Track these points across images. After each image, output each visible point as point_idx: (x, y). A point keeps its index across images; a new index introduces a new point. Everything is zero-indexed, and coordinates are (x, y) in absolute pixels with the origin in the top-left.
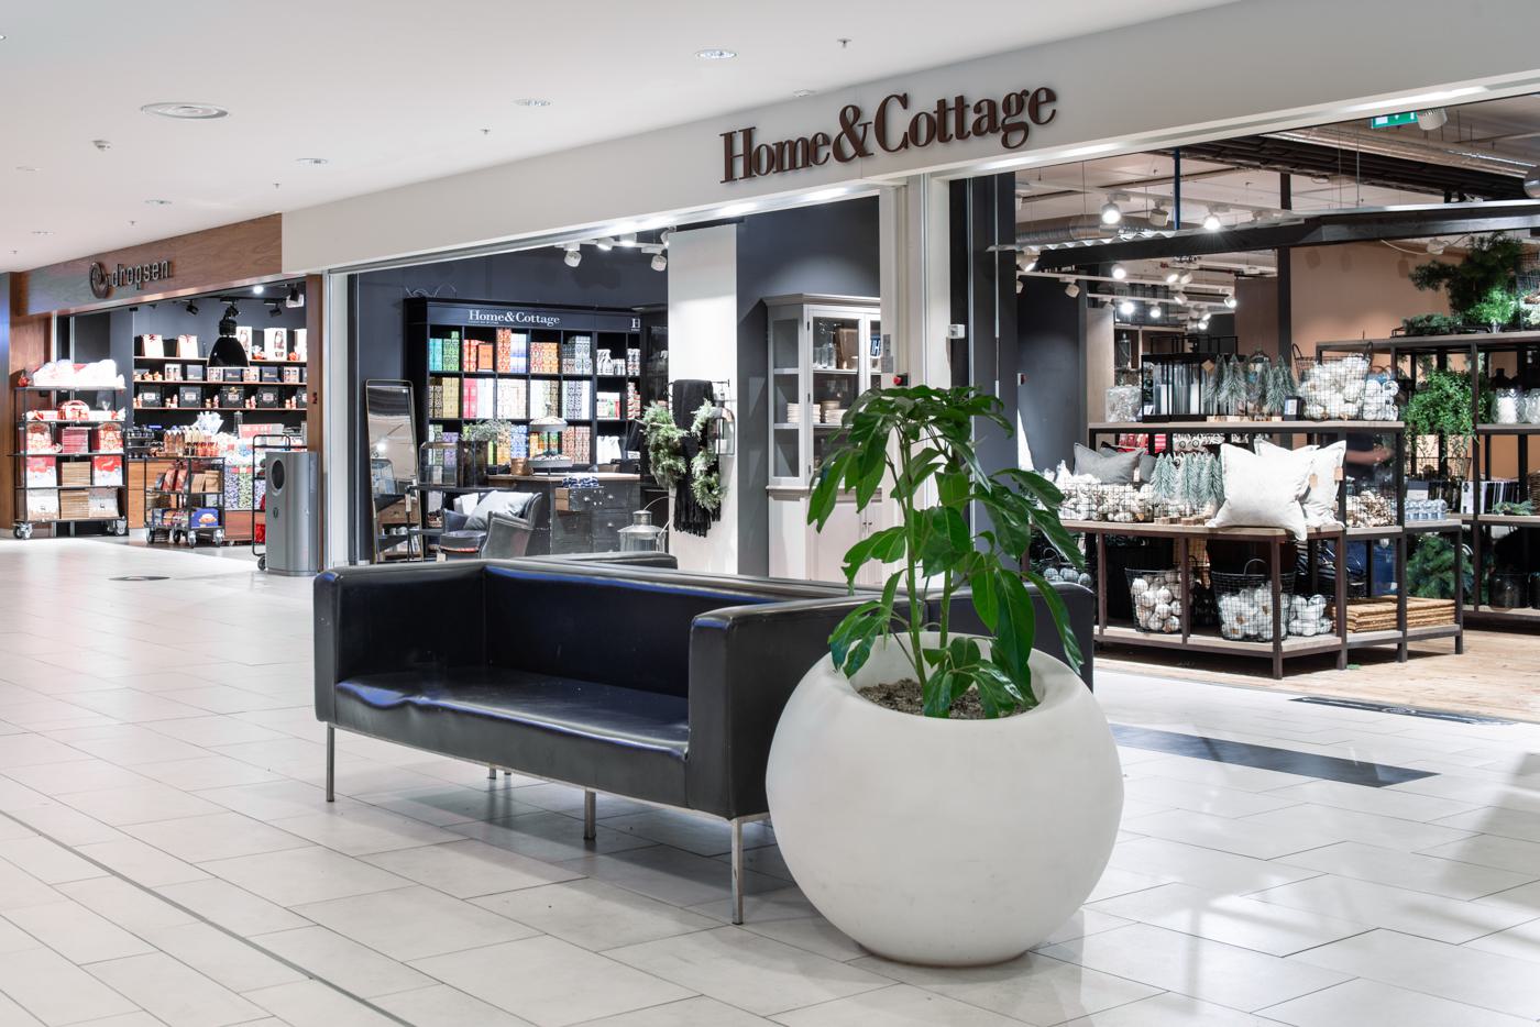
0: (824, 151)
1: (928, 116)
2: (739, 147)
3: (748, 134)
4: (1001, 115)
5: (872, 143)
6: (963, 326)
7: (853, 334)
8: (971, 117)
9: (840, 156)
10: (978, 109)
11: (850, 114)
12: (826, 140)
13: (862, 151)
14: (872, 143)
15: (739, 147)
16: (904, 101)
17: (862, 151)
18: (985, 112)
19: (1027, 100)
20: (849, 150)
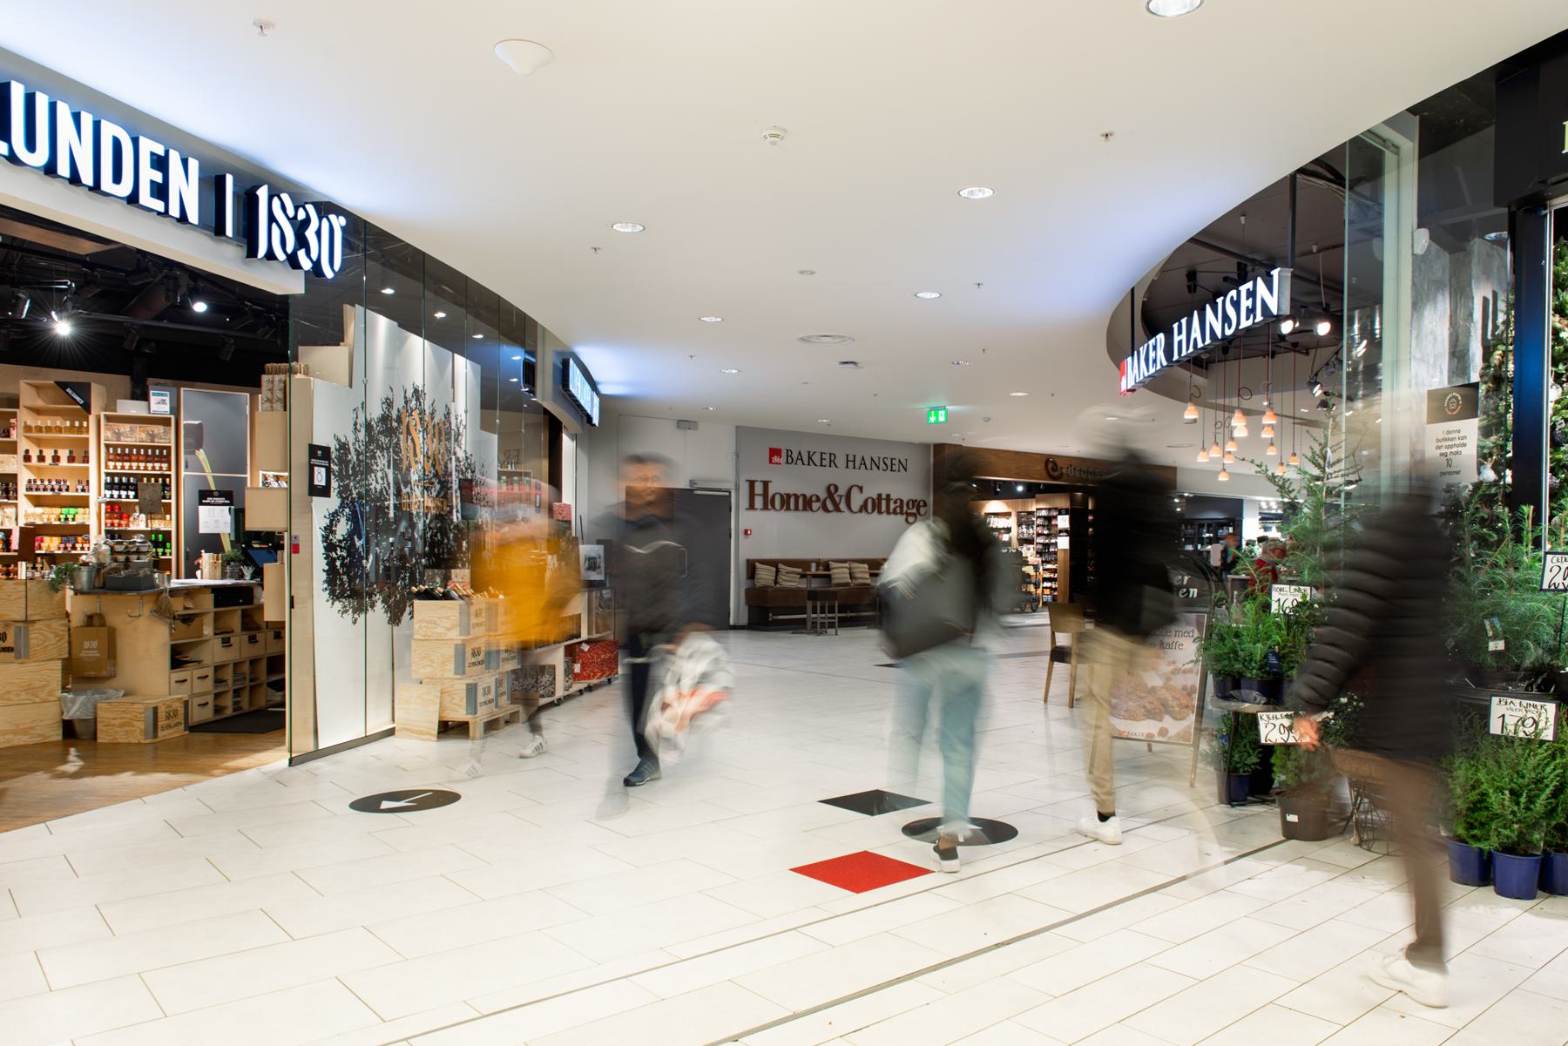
0: (815, 505)
1: (873, 499)
2: (759, 489)
3: (766, 484)
4: (905, 508)
5: (843, 506)
6: (316, 483)
7: (834, 609)
8: (892, 506)
9: (826, 509)
10: (1266, 529)
11: (832, 489)
12: (818, 499)
13: (837, 509)
14: (843, 506)
15: (759, 489)
16: (861, 489)
17: (837, 509)
18: (898, 504)
19: (916, 504)
20: (830, 506)
